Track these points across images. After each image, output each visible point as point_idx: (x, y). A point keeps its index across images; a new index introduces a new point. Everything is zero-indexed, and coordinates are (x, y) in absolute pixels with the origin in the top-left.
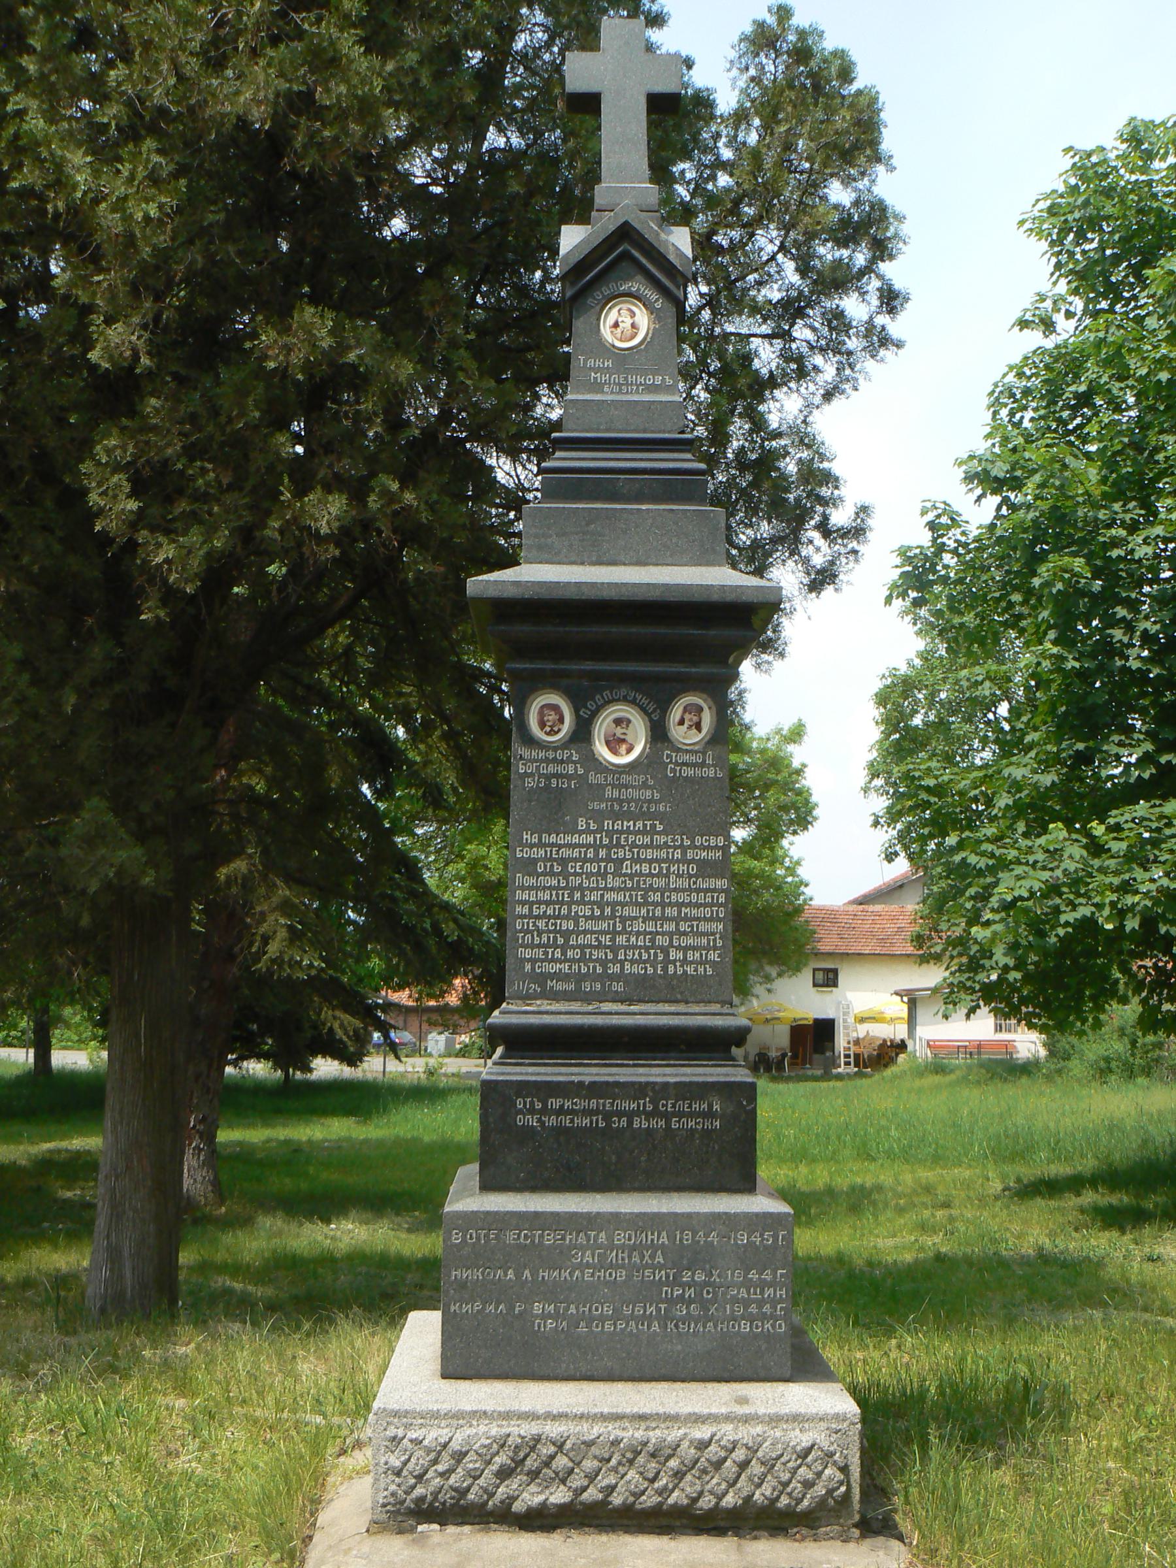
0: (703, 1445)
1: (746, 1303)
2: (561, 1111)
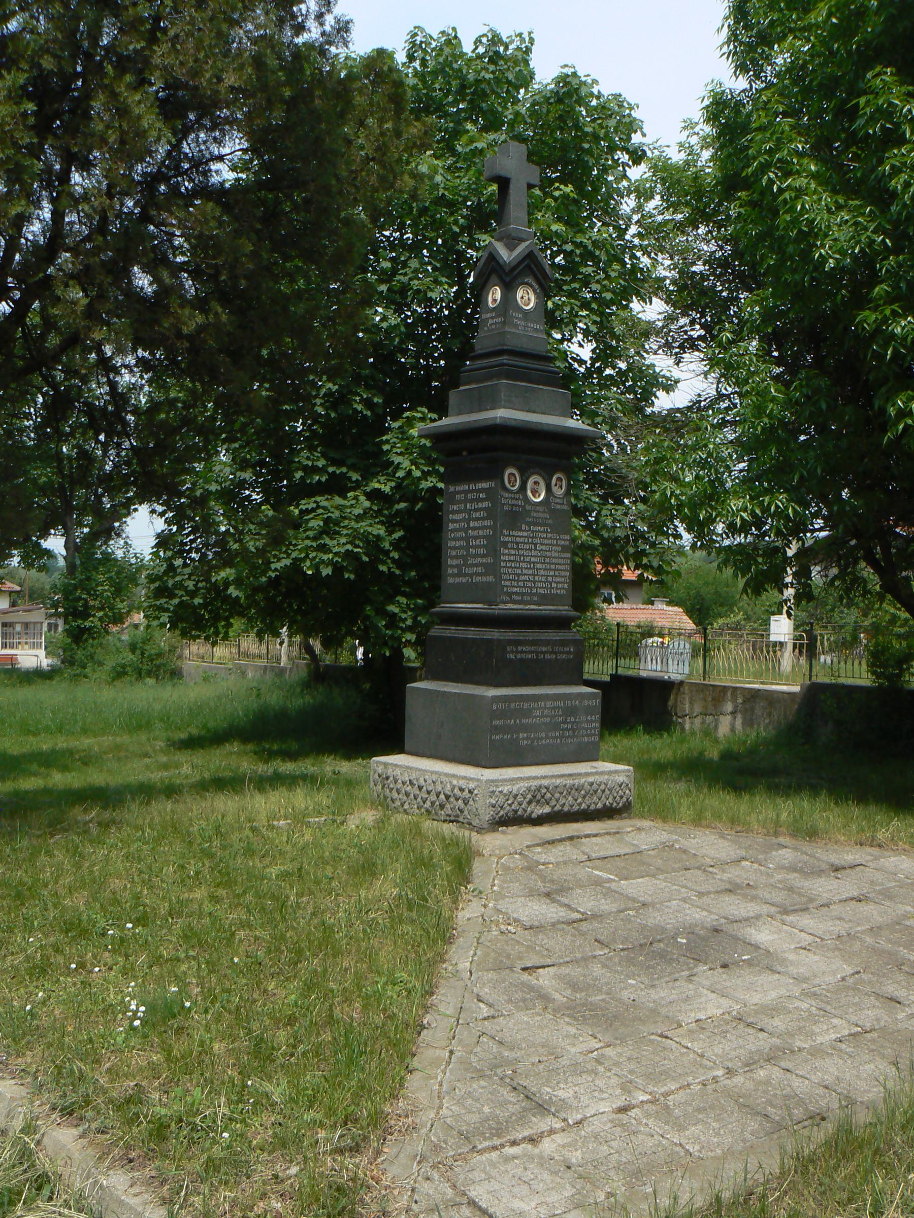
0: (591, 784)
1: (586, 729)
2: (522, 652)
